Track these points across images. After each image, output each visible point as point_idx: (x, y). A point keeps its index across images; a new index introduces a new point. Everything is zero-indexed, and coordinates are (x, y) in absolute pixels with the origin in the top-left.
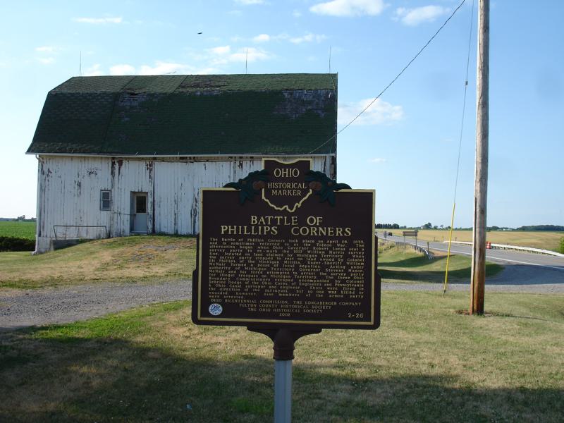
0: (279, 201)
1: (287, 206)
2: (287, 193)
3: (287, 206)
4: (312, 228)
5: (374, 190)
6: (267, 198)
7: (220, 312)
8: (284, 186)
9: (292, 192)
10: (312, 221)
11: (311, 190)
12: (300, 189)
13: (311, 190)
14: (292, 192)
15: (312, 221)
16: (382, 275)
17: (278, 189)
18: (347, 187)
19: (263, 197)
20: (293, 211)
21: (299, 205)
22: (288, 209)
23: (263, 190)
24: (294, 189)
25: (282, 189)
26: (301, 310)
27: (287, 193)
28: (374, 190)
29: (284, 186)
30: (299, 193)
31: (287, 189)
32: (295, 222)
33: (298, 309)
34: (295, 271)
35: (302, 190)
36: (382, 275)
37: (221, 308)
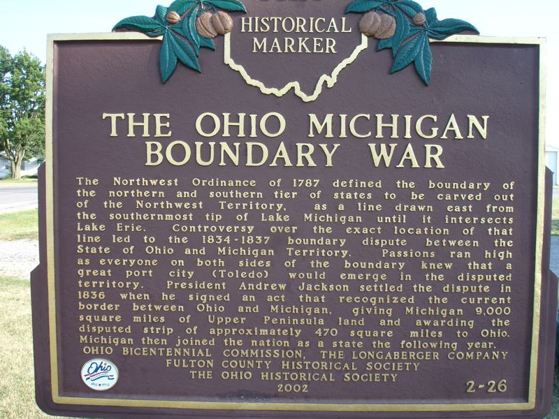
0: (272, 68)
1: (296, 84)
2: (296, 47)
3: (296, 84)
4: (428, 147)
5: (49, 36)
6: (237, 62)
7: (112, 383)
8: (289, 24)
9: (310, 44)
10: (208, 123)
11: (365, 39)
12: (332, 34)
13: (365, 39)
14: (310, 44)
15: (208, 123)
16: (84, 264)
17: (271, 36)
18: (471, 30)
19: (228, 60)
20: (313, 97)
21: (332, 81)
22: (298, 92)
23: (227, 37)
24: (316, 34)
25: (281, 35)
26: (257, 373)
27: (296, 47)
28: (49, 36)
29: (289, 24)
30: (331, 47)
31: (295, 35)
32: (164, 130)
33: (327, 372)
34: (406, 271)
35: (340, 37)
36: (84, 264)
37: (114, 371)
